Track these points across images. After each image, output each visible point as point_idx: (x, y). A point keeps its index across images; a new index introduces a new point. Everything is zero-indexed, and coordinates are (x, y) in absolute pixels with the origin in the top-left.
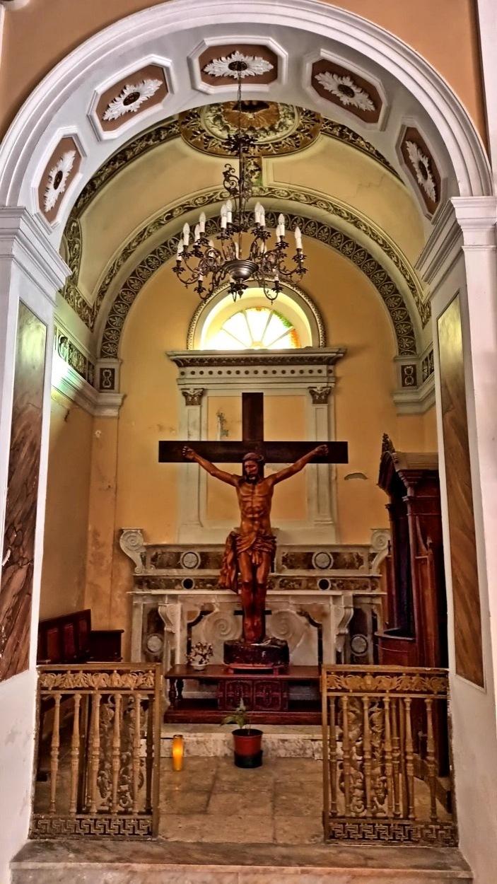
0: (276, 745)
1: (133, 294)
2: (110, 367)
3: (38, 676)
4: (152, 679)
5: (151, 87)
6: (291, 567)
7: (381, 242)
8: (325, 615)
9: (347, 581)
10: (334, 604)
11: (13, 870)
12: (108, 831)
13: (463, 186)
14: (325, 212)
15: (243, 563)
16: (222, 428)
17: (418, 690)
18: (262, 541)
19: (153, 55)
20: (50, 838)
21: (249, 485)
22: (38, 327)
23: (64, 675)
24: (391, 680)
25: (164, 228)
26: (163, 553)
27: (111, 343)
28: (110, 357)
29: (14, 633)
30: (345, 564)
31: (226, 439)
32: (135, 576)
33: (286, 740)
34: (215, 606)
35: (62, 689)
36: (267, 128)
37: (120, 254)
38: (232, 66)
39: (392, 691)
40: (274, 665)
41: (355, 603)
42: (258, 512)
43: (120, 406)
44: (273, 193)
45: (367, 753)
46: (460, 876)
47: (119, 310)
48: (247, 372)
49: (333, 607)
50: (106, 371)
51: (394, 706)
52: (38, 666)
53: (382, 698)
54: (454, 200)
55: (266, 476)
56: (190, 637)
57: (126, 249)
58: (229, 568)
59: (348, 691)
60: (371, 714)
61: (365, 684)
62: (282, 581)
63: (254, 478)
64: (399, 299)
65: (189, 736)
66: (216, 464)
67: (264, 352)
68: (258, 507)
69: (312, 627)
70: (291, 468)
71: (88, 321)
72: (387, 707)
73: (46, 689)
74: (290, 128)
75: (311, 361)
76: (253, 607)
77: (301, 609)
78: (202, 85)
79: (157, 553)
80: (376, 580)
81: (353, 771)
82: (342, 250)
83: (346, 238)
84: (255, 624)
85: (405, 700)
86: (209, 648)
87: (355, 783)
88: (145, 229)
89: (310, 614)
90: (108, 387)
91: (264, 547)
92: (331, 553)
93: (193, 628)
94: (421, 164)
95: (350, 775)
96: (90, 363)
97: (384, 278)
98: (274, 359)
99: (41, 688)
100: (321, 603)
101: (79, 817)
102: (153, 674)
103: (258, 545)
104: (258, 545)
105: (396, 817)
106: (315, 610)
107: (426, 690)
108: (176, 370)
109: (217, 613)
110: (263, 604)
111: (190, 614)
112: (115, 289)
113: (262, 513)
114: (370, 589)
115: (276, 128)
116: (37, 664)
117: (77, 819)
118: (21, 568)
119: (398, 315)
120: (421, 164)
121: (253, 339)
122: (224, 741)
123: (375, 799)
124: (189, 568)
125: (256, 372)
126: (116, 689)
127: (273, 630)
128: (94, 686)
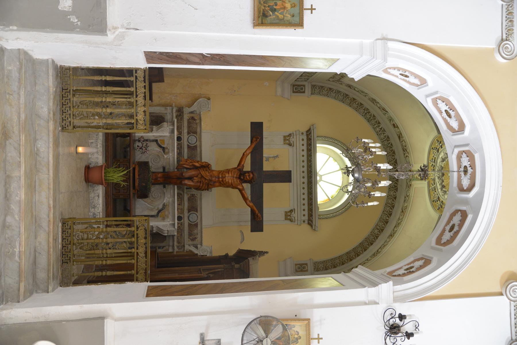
2: (306, 91)
4: (142, 128)
5: (455, 124)
6: (189, 199)
7: (379, 250)
8: (163, 219)
10: (170, 224)
11: (48, 60)
12: (64, 106)
13: (398, 287)
14: (397, 218)
15: (192, 173)
16: (270, 157)
19: (470, 126)
22: (326, 66)
24: (143, 253)
25: (388, 122)
26: (196, 124)
29: (168, 58)
31: (264, 159)
35: (136, 82)
36: (443, 183)
37: (372, 97)
38: (465, 167)
39: (137, 253)
41: (169, 236)
42: (222, 181)
44: (409, 187)
46: (50, 287)
48: (303, 183)
49: (168, 223)
51: (129, 254)
53: (134, 248)
54: (391, 283)
57: (375, 100)
59: (137, 231)
62: (181, 194)
63: (242, 178)
66: (249, 156)
67: (316, 183)
70: (248, 199)
72: (129, 251)
73: (136, 72)
74: (443, 197)
75: (310, 210)
76: (167, 179)
78: (456, 151)
80: (183, 249)
81: (97, 233)
82: (376, 227)
83: (382, 230)
88: (387, 112)
91: (203, 184)
93: (155, 143)
94: (412, 267)
96: (308, 79)
98: (311, 188)
99: (136, 70)
100: (170, 217)
101: (71, 91)
105: (74, 255)
106: (166, 213)
108: (304, 129)
110: (170, 183)
111: (163, 141)
113: (222, 182)
115: (444, 189)
118: (201, 60)
119: (338, 261)
120: (412, 267)
125: (304, 205)
127: (155, 190)
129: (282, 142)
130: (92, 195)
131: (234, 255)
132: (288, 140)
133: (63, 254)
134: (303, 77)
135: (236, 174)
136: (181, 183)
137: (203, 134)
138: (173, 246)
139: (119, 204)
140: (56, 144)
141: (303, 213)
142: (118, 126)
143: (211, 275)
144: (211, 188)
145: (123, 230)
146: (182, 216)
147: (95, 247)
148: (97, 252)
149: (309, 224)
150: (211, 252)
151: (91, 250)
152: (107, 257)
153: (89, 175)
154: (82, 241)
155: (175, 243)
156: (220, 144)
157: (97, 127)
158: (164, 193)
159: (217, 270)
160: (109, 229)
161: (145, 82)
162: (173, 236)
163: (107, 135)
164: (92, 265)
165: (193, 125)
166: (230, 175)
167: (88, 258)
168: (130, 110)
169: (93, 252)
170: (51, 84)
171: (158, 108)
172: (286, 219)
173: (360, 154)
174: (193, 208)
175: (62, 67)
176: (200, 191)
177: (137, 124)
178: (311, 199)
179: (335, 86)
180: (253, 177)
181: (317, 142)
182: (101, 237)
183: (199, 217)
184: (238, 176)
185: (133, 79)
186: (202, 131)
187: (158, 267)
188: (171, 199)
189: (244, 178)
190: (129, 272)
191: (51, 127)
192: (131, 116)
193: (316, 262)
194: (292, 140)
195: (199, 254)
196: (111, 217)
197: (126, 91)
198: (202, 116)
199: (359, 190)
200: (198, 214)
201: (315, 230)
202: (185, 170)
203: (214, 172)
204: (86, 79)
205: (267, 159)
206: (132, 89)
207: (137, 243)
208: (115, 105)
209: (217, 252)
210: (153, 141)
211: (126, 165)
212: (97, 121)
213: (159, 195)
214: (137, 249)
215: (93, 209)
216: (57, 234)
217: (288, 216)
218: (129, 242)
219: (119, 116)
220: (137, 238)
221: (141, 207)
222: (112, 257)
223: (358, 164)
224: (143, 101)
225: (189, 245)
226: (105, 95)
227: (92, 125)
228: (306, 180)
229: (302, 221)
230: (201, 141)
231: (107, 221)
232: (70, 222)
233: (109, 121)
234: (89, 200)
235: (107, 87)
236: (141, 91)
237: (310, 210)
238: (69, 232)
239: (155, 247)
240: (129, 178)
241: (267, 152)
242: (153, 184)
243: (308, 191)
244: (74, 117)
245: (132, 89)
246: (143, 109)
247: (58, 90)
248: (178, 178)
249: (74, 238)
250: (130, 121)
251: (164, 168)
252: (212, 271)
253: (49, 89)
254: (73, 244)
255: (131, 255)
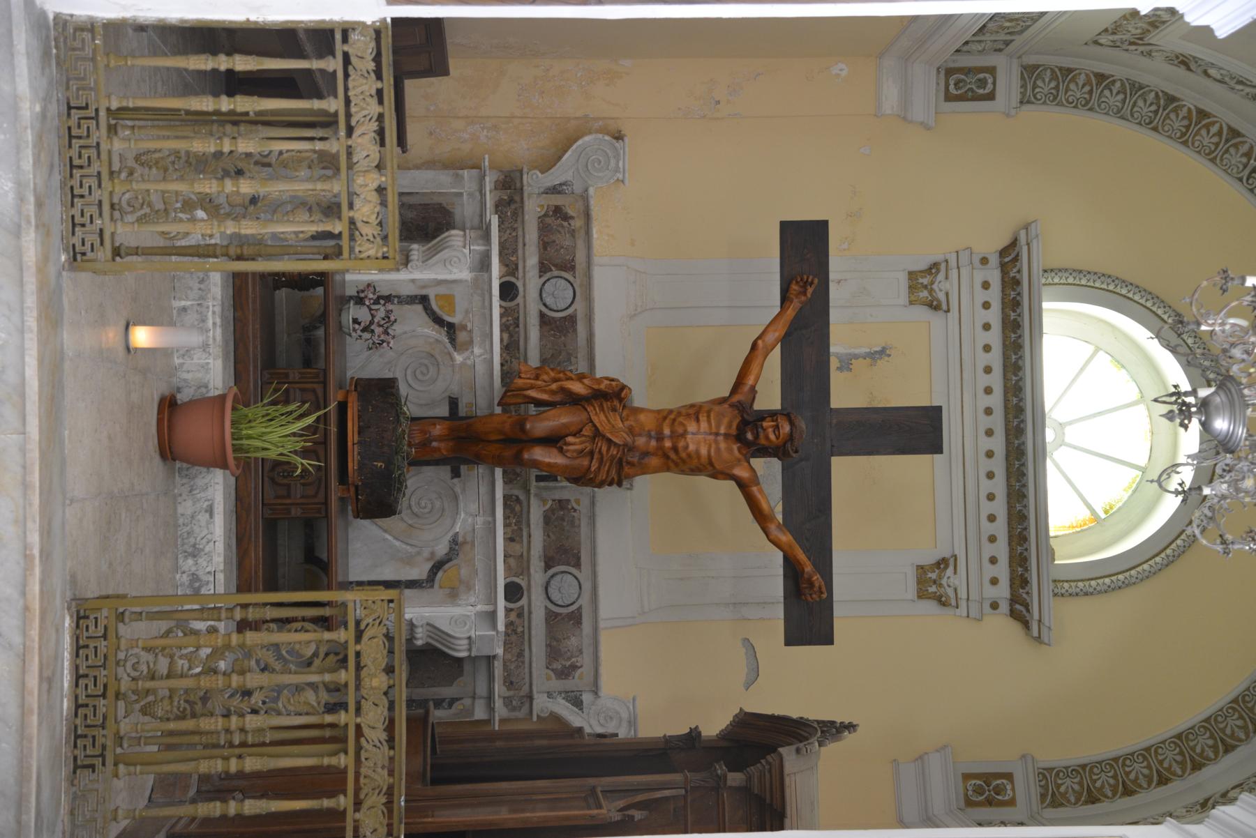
0: (202, 495)
1: (1183, 134)
3: (369, 23)
4: (372, 252)
6: (547, 520)
8: (453, 595)
9: (523, 643)
10: (478, 614)
12: (77, 173)
16: (856, 357)
17: (362, 780)
18: (613, 457)
20: (58, 56)
21: (734, 426)
23: (373, 75)
24: (381, 726)
26: (573, 233)
27: (1057, 88)
28: (1024, 86)
30: (558, 641)
31: (834, 363)
32: (521, 171)
33: (211, 516)
34: (467, 354)
35: (346, 75)
40: (357, 488)
41: (473, 660)
42: (675, 449)
43: (905, 119)
45: (241, 678)
47: (1140, 103)
48: (990, 454)
49: (470, 611)
50: (990, 81)
51: (328, 733)
52: (389, 20)
55: (753, 461)
56: (400, 303)
58: (554, 386)
60: (312, 686)
61: (372, 676)
62: (518, 500)
63: (749, 436)
64: (1179, 772)
65: (214, 313)
66: (776, 353)
67: (1041, 453)
68: (687, 447)
69: (428, 566)
71: (1114, 33)
72: (329, 719)
73: (345, 39)
75: (1019, 561)
76: (467, 442)
77: (465, 543)
79: (572, 218)
84: (435, 444)
85: (342, 756)
86: (383, 341)
87: (181, 657)
89: (454, 562)
90: (952, 87)
91: (601, 461)
92: (580, 607)
93: (419, 308)
95: (198, 648)
96: (1007, 43)
97: (1232, 736)
98: (1022, 474)
99: (347, 30)
100: (479, 586)
101: (102, 113)
102: (380, 255)
103: (604, 449)
104: (604, 449)
105: (119, 739)
106: (464, 572)
107: (362, 796)
109: (452, 359)
110: (477, 459)
111: (449, 300)
112: (1192, 91)
113: (672, 455)
114: (508, 694)
116: (393, 19)
117: (97, 110)
121: (1070, 423)
122: (206, 387)
123: (151, 698)
124: (541, 295)
126: (350, 181)
127: (421, 485)
128: (354, 136)
129: (904, 297)
130: (186, 507)
131: (725, 735)
132: (924, 287)
133: (76, 736)
134: (988, 37)
135: (726, 421)
136: (518, 459)
137: (597, 272)
138: (490, 698)
139: (288, 541)
140: (51, 316)
141: (990, 571)
142: (281, 248)
143: (638, 815)
144: (630, 477)
145: (306, 640)
146: (523, 584)
147: (198, 707)
148: (206, 724)
149: (1014, 614)
150: (632, 722)
151: (182, 717)
152: (243, 744)
153: (173, 429)
154: (150, 684)
155: (498, 688)
156: (666, 308)
157: (203, 252)
158: (456, 498)
159: (658, 795)
160: (251, 637)
161: (379, 77)
162: (490, 659)
163: (239, 283)
164: (188, 776)
165: (561, 239)
166: (704, 425)
167: (170, 747)
168: (326, 186)
169: (189, 724)
170: (23, 86)
171: (428, 175)
172: (922, 595)
173: (1238, 338)
174: (565, 552)
175: (62, 22)
176: (588, 490)
177: (352, 238)
178: (1023, 518)
179: (1124, 65)
180: (793, 434)
181: (1046, 291)
182: (222, 665)
183: (587, 586)
184: (734, 431)
185: (333, 64)
186: (596, 259)
187: (435, 781)
188: (480, 520)
189: (757, 436)
190: (326, 803)
191: (31, 253)
192: (331, 209)
193: (1050, 770)
194: (942, 286)
195: (587, 730)
196: (257, 591)
197: (312, 112)
198: (592, 202)
199: (1235, 484)
200: (584, 574)
201: (1038, 639)
202: (532, 409)
203: (642, 417)
204: (157, 69)
205: (846, 365)
206: (332, 105)
207: (358, 687)
208: (269, 165)
209: (657, 724)
210: (412, 300)
211: (314, 391)
212: (201, 229)
213: (438, 504)
214: (358, 710)
215: (190, 561)
216: (57, 657)
217: (931, 582)
218: (326, 685)
219: (277, 208)
220: (359, 668)
221: (367, 549)
222: (263, 744)
223: (1230, 378)
224: (374, 150)
225: (550, 695)
226: (229, 128)
227: (183, 243)
228: (998, 444)
229: (987, 606)
230: (589, 300)
231: (245, 606)
232: (105, 612)
233: (249, 228)
234: (176, 526)
235: (238, 98)
236: (366, 110)
237: (1019, 561)
238: (102, 649)
239: (423, 703)
240: (325, 442)
241: (843, 336)
242: (413, 463)
243: (1009, 486)
244: (117, 214)
245: (332, 105)
246: (374, 180)
247: (53, 109)
248: (508, 441)
249: (120, 670)
250: (328, 227)
251: (453, 403)
252: (640, 798)
253: (15, 108)
254: (118, 695)
255: (337, 738)
